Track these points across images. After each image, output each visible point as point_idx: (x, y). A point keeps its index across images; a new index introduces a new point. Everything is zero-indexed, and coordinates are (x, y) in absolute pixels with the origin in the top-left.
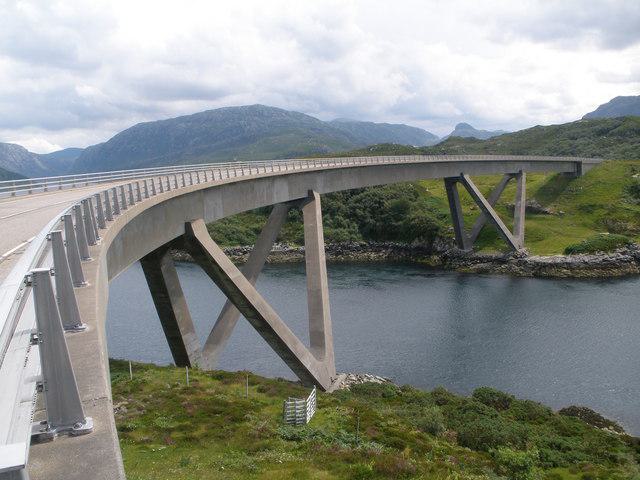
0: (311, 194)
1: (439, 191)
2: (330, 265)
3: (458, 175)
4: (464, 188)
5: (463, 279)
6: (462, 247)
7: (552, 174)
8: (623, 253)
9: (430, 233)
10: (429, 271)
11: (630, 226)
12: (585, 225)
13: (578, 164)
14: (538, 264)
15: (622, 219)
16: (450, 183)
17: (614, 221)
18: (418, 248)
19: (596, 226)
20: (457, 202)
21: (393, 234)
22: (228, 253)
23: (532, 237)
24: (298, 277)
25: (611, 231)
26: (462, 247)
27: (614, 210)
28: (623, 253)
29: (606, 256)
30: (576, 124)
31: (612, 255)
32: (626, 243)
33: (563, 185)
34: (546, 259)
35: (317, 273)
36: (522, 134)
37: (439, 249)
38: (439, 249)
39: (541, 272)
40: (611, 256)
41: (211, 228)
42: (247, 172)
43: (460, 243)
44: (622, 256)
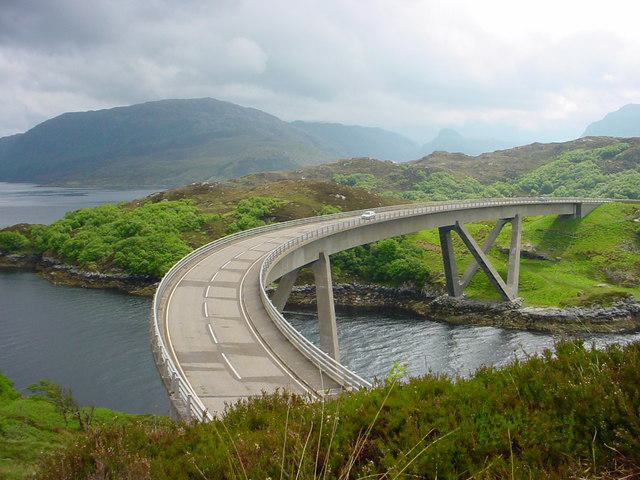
0: (321, 255)
1: (430, 235)
2: (338, 309)
5: (452, 325)
7: (555, 216)
8: (620, 307)
9: (418, 279)
10: (412, 317)
11: (629, 275)
13: (578, 206)
14: (531, 316)
15: (621, 268)
16: (444, 232)
17: (613, 269)
19: (590, 275)
21: (382, 278)
25: (610, 281)
27: (611, 259)
28: (620, 307)
31: (609, 308)
34: (539, 311)
35: (327, 312)
37: (428, 295)
38: (428, 295)
40: (607, 310)
41: (296, 284)
43: (450, 289)
44: (618, 311)
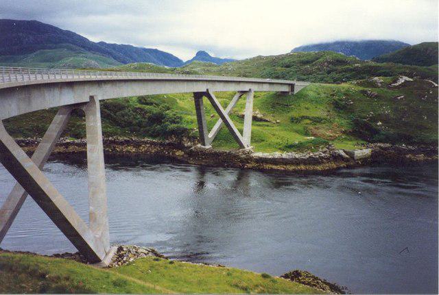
1: (189, 104)
3: (205, 90)
4: (209, 102)
6: (204, 145)
8: (325, 152)
9: (182, 133)
12: (297, 132)
18: (169, 144)
20: (73, 71)
22: (19, 143)
23: (255, 139)
24: (81, 172)
26: (204, 145)
28: (325, 152)
29: (311, 154)
30: (287, 55)
32: (326, 143)
33: (279, 102)
36: (246, 62)
39: (261, 166)
42: (32, 77)
44: (323, 155)
